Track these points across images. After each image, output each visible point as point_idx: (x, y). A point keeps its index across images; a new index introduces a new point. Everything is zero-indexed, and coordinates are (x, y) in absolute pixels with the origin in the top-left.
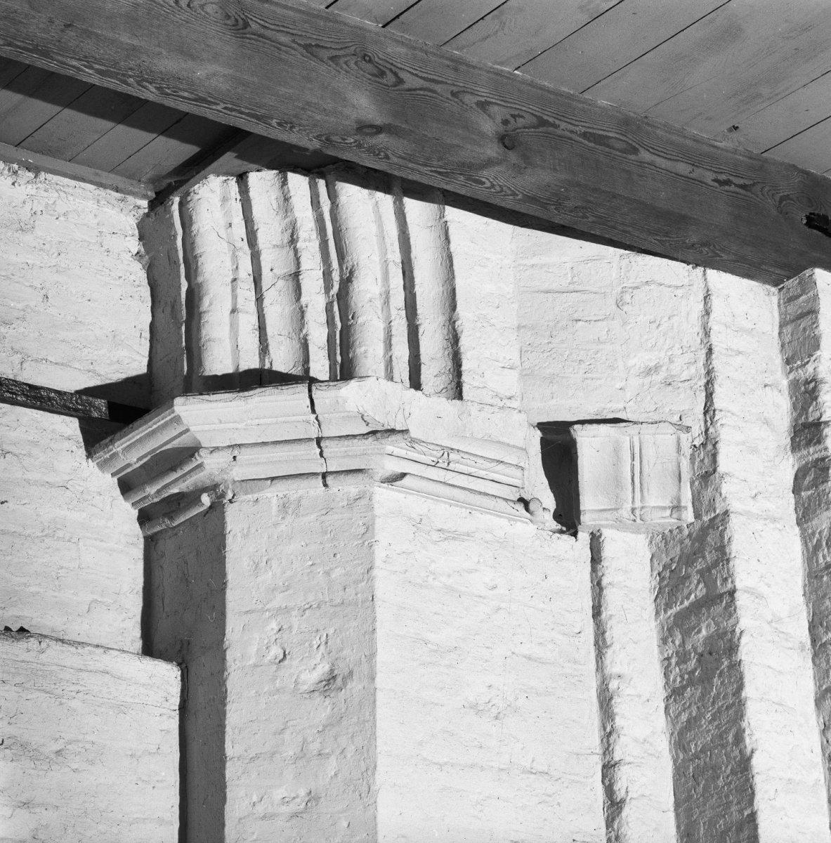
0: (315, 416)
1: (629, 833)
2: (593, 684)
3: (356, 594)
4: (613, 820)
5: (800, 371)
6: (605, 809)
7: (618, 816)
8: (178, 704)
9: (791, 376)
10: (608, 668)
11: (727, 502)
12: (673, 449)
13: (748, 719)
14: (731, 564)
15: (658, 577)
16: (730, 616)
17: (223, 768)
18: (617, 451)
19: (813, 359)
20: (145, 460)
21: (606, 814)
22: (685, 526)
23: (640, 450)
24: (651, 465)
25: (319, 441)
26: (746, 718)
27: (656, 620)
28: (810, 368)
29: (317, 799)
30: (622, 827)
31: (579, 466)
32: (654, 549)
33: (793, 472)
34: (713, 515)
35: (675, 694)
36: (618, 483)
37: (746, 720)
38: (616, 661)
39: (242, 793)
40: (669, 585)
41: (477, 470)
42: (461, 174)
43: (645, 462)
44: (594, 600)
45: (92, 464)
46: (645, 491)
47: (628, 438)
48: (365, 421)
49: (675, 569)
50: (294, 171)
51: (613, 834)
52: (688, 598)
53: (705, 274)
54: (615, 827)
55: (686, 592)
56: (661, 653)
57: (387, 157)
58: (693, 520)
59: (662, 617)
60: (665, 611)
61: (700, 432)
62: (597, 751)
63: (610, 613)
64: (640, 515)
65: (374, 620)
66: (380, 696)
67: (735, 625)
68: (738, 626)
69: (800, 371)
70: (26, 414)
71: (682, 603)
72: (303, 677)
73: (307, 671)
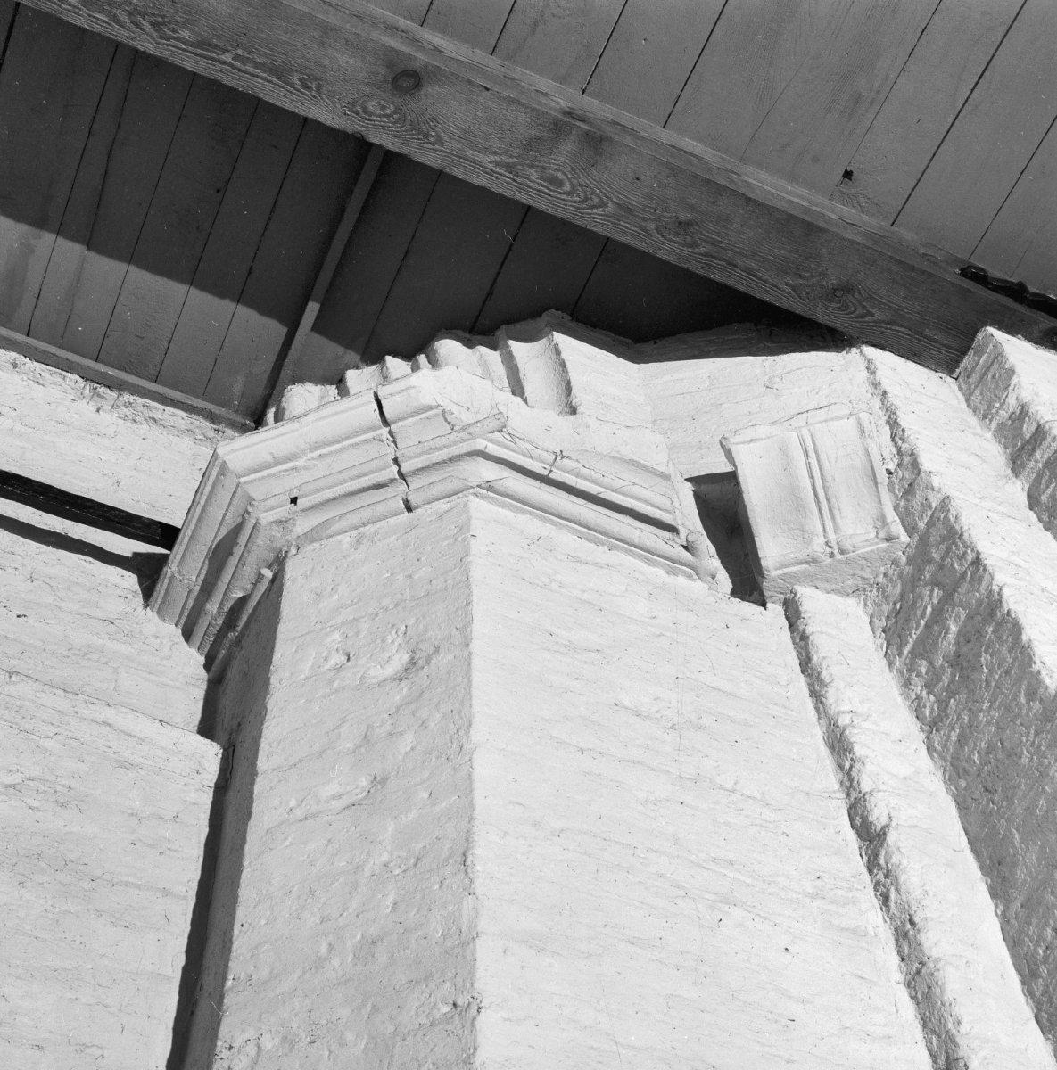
0: (388, 429)
1: (905, 862)
2: (818, 734)
3: (446, 582)
4: (876, 856)
5: (1001, 412)
6: (863, 853)
7: (882, 845)
8: (214, 781)
9: (994, 425)
10: (833, 707)
11: (943, 491)
12: (854, 433)
13: (1040, 657)
14: (966, 536)
15: (883, 634)
16: (980, 580)
17: (252, 783)
18: (785, 452)
19: (1011, 388)
20: (204, 572)
21: (865, 858)
22: (900, 553)
23: (813, 440)
24: (833, 461)
25: (505, 832)
26: (1036, 659)
27: (891, 671)
28: (1012, 401)
29: (384, 781)
30: (891, 857)
31: (747, 502)
32: (870, 609)
33: (1025, 494)
34: (929, 513)
35: (932, 725)
36: (799, 507)
37: (1038, 661)
38: (841, 699)
39: (276, 801)
40: (898, 629)
41: (605, 490)
42: (531, 166)
43: (823, 457)
44: (799, 654)
45: (151, 614)
46: (836, 512)
47: (795, 434)
48: (449, 423)
49: (901, 608)
50: (395, 355)
51: (881, 876)
52: (923, 616)
53: (861, 352)
54: (882, 861)
55: (919, 612)
56: (907, 698)
57: (440, 141)
58: (908, 539)
59: (897, 664)
60: (900, 655)
61: (892, 456)
62: (838, 795)
63: (821, 655)
64: (838, 543)
65: (470, 595)
66: (477, 662)
67: (991, 584)
68: (994, 583)
69: (1001, 412)
70: (70, 557)
71: (918, 625)
72: (372, 672)
73: (379, 667)
